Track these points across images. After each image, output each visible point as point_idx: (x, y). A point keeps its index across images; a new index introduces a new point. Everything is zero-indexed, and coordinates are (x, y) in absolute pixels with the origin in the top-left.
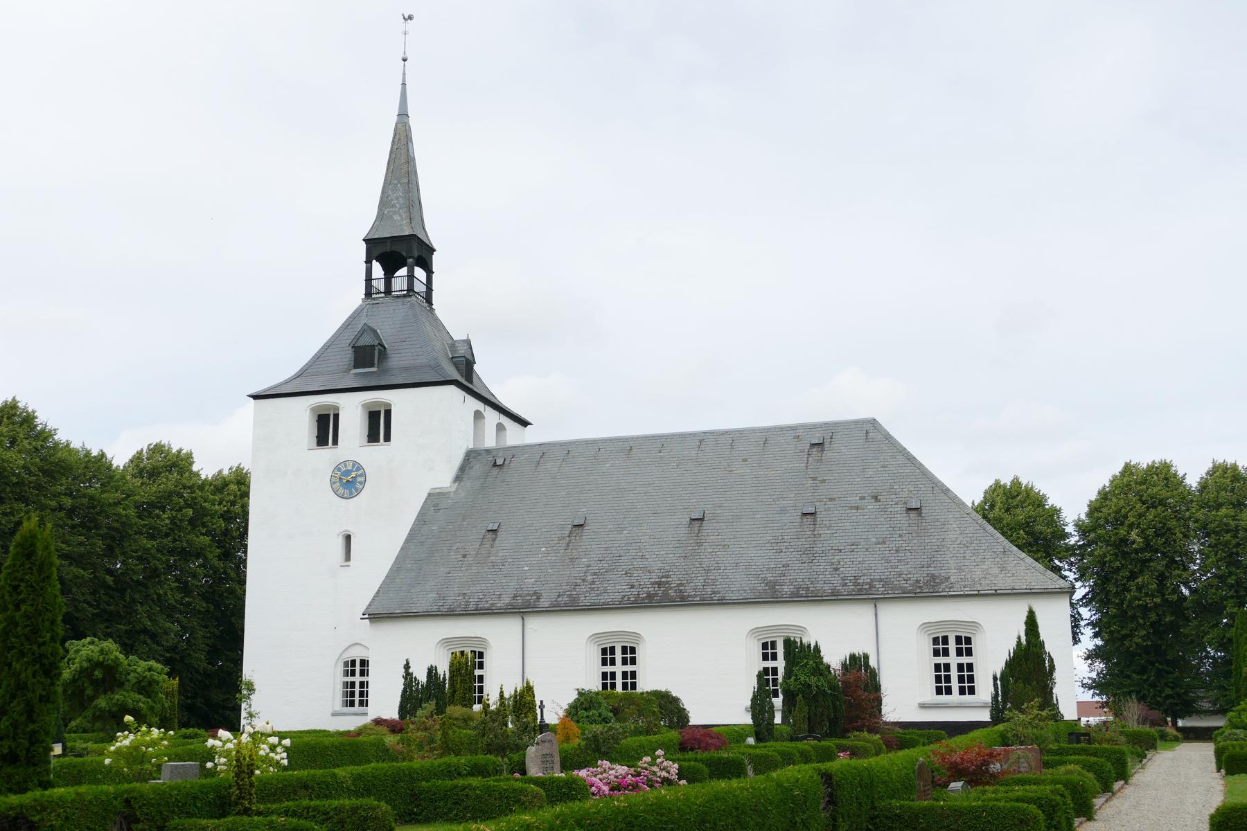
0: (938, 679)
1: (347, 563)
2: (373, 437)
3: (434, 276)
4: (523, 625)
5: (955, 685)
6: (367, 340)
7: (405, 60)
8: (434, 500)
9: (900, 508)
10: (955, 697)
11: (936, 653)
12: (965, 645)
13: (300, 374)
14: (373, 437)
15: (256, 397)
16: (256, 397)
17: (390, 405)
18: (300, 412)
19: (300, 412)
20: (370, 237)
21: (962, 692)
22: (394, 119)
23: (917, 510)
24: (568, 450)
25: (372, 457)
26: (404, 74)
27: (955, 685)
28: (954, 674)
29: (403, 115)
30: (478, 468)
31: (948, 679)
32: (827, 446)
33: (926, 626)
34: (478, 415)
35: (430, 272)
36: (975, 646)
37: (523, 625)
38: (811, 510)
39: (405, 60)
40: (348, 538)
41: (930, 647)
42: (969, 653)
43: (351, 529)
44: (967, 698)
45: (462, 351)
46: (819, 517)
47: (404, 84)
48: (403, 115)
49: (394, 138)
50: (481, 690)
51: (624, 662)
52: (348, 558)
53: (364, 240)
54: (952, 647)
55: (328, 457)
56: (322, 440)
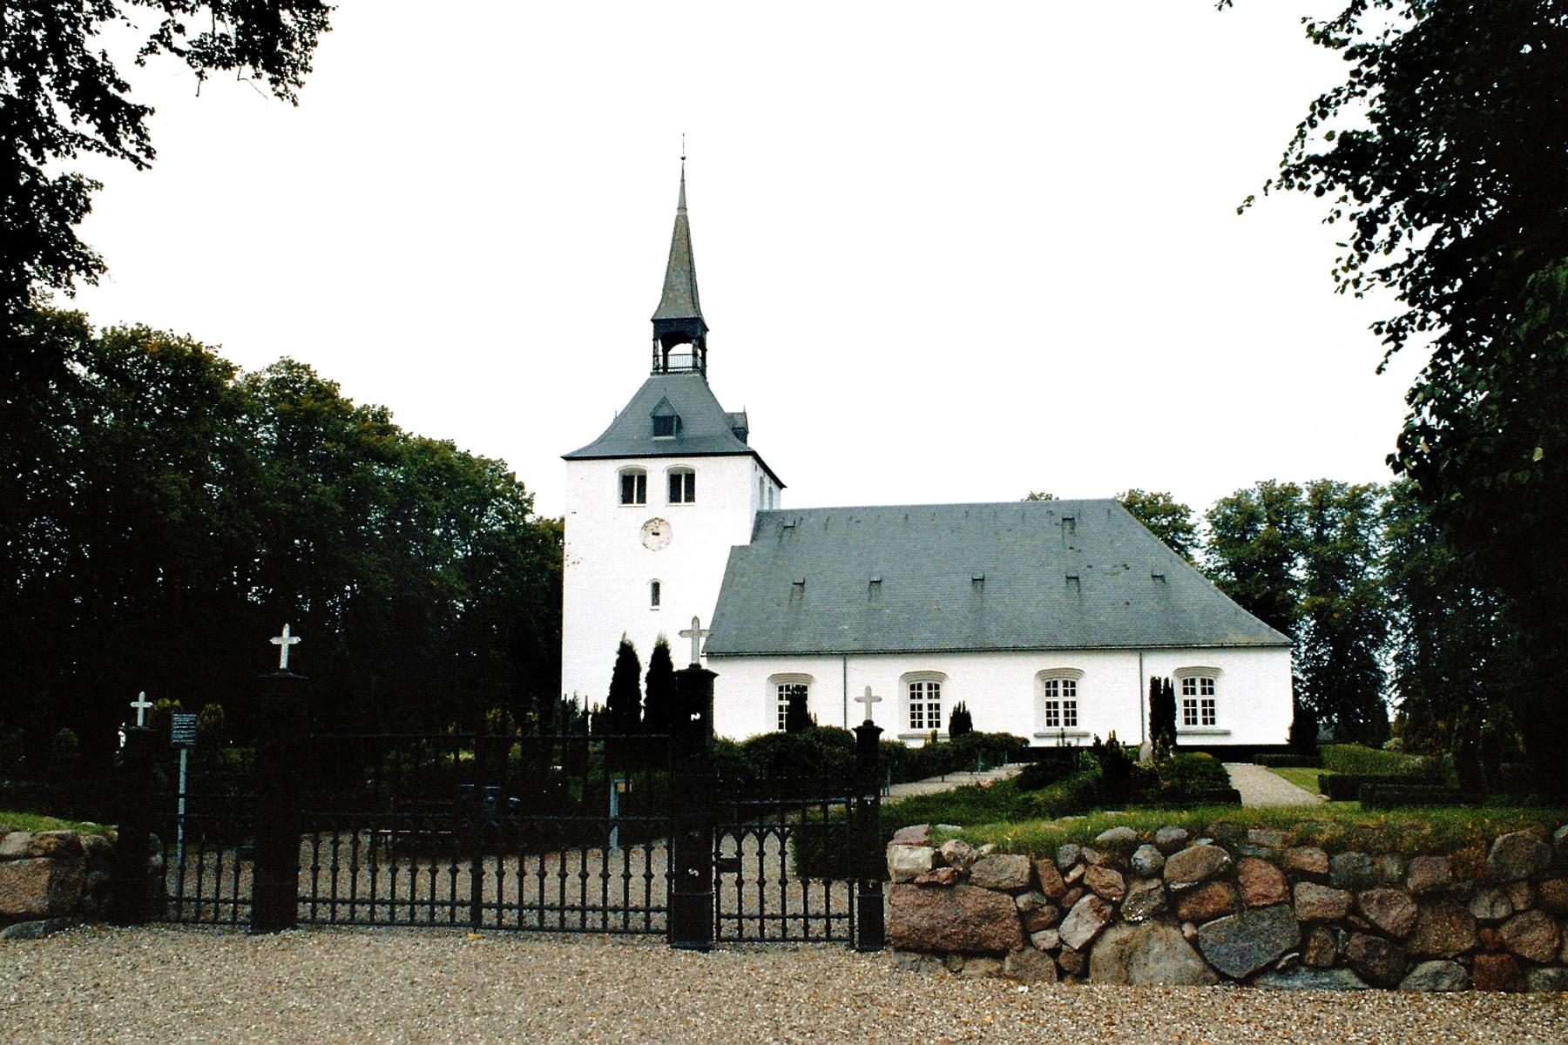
0: (1049, 714)
1: (655, 607)
2: (674, 497)
3: (707, 353)
4: (845, 664)
5: (1200, 717)
6: (664, 412)
7: (683, 159)
8: (737, 553)
9: (1148, 575)
10: (1200, 726)
11: (1048, 694)
12: (935, 690)
13: (601, 440)
14: (674, 497)
15: (567, 458)
16: (567, 458)
17: (645, 472)
18: (609, 474)
19: (609, 474)
20: (657, 318)
21: (1205, 722)
22: (675, 213)
23: (1162, 577)
24: (829, 517)
26: (683, 181)
27: (1200, 717)
28: (1061, 709)
29: (683, 207)
30: (770, 528)
31: (1205, 712)
32: (1077, 520)
33: (774, 678)
35: (704, 350)
36: (1216, 687)
37: (845, 664)
38: (1075, 575)
39: (683, 159)
42: (1211, 692)
43: (659, 577)
44: (1209, 727)
45: (740, 424)
46: (806, 585)
47: (683, 181)
48: (683, 207)
49: (675, 228)
50: (781, 717)
51: (1204, 692)
53: (652, 320)
54: (925, 691)
56: (627, 498)
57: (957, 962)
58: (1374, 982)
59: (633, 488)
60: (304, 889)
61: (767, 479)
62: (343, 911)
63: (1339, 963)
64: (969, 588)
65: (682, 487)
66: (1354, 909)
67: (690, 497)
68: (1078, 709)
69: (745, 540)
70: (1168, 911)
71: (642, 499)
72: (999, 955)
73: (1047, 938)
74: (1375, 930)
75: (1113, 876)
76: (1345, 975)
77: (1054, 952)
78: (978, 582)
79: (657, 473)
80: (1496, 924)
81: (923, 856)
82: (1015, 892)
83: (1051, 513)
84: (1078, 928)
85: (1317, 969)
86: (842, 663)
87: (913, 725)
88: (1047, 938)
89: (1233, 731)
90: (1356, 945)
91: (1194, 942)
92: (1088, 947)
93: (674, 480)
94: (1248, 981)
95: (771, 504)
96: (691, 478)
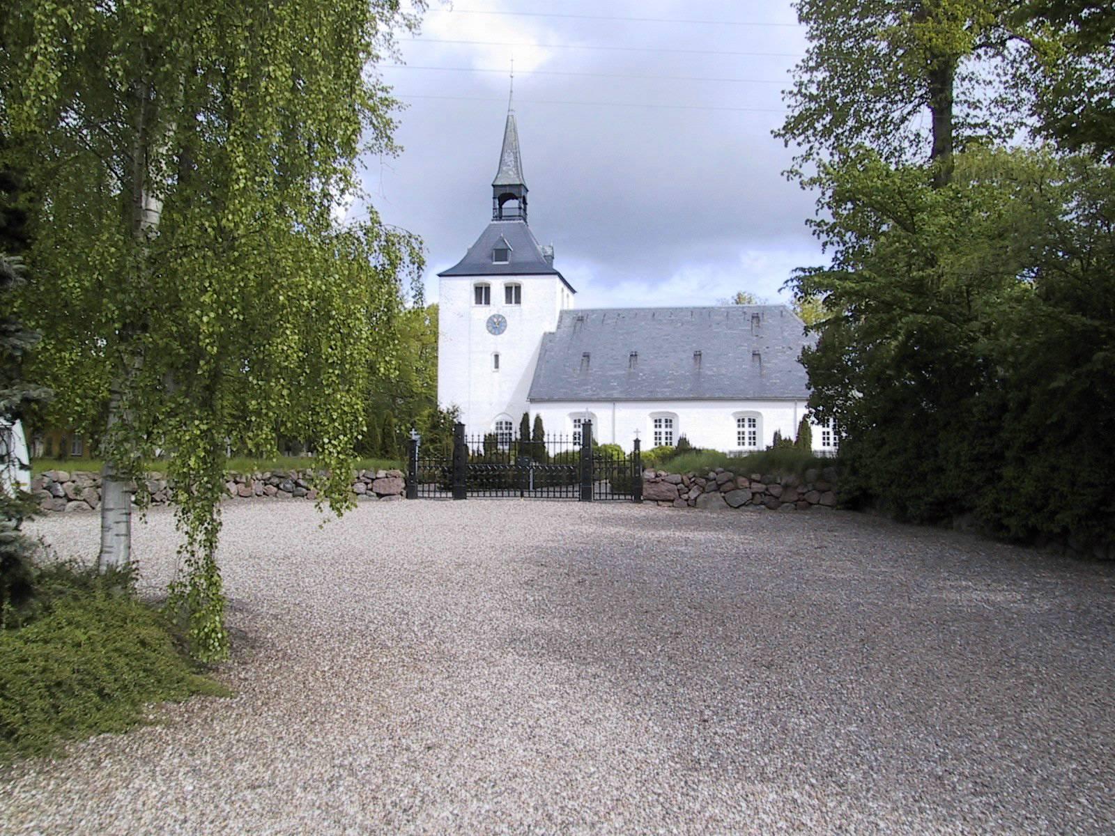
5: (747, 441)
14: (509, 300)
15: (440, 275)
18: (466, 285)
21: (750, 444)
25: (509, 311)
27: (747, 441)
34: (563, 290)
40: (497, 356)
41: (736, 424)
52: (497, 367)
55: (484, 312)
56: (478, 301)
57: (660, 503)
58: (770, 508)
59: (482, 294)
60: (597, 491)
61: (566, 289)
62: (603, 497)
63: (762, 503)
64: (692, 361)
65: (513, 294)
66: (767, 489)
67: (518, 301)
68: (822, 441)
69: (553, 328)
70: (718, 488)
71: (488, 302)
72: (672, 501)
73: (686, 496)
74: (771, 495)
75: (703, 480)
76: (763, 506)
77: (687, 500)
78: (698, 355)
79: (497, 285)
80: (804, 494)
81: (652, 475)
82: (676, 484)
83: (745, 313)
84: (693, 494)
85: (756, 505)
86: (793, 410)
87: (739, 444)
88: (686, 496)
89: (776, 429)
90: (766, 499)
91: (724, 497)
92: (696, 499)
93: (508, 289)
94: (738, 508)
95: (146, 205)
96: (518, 288)
